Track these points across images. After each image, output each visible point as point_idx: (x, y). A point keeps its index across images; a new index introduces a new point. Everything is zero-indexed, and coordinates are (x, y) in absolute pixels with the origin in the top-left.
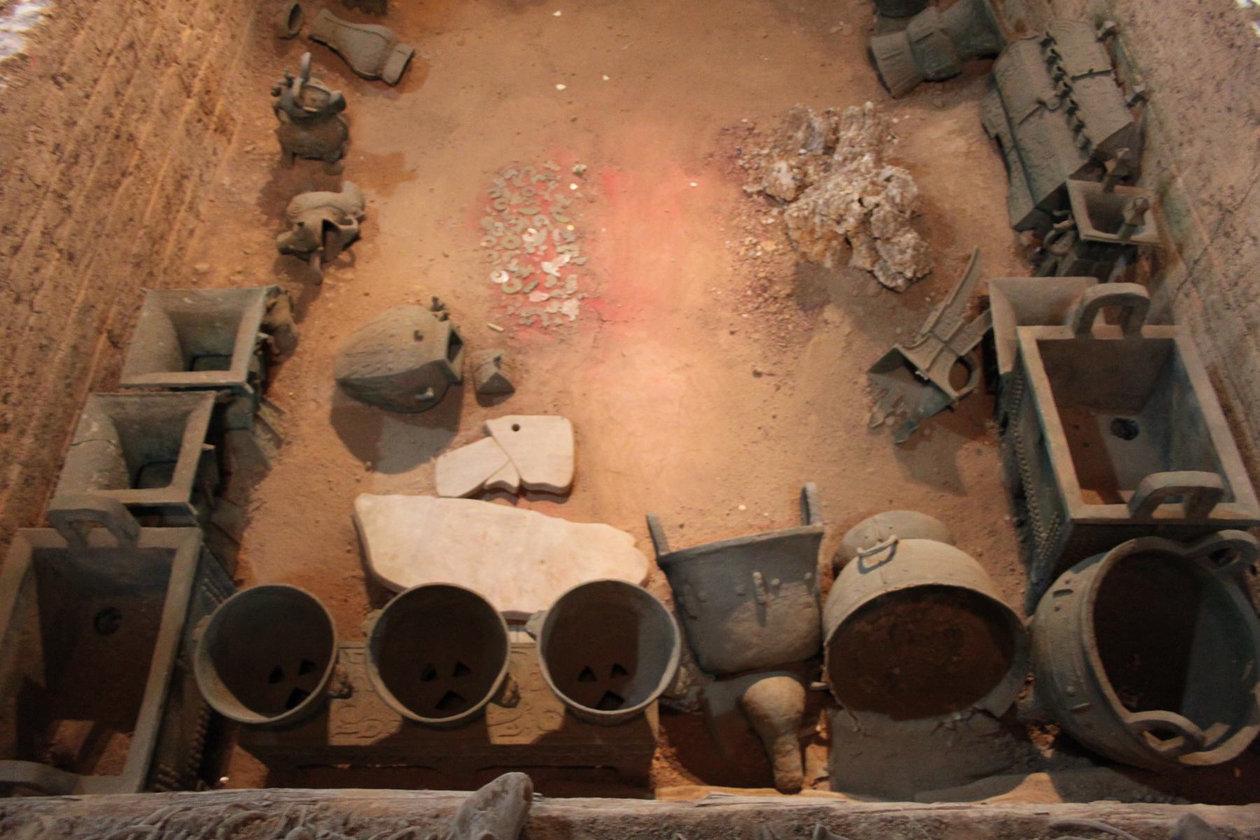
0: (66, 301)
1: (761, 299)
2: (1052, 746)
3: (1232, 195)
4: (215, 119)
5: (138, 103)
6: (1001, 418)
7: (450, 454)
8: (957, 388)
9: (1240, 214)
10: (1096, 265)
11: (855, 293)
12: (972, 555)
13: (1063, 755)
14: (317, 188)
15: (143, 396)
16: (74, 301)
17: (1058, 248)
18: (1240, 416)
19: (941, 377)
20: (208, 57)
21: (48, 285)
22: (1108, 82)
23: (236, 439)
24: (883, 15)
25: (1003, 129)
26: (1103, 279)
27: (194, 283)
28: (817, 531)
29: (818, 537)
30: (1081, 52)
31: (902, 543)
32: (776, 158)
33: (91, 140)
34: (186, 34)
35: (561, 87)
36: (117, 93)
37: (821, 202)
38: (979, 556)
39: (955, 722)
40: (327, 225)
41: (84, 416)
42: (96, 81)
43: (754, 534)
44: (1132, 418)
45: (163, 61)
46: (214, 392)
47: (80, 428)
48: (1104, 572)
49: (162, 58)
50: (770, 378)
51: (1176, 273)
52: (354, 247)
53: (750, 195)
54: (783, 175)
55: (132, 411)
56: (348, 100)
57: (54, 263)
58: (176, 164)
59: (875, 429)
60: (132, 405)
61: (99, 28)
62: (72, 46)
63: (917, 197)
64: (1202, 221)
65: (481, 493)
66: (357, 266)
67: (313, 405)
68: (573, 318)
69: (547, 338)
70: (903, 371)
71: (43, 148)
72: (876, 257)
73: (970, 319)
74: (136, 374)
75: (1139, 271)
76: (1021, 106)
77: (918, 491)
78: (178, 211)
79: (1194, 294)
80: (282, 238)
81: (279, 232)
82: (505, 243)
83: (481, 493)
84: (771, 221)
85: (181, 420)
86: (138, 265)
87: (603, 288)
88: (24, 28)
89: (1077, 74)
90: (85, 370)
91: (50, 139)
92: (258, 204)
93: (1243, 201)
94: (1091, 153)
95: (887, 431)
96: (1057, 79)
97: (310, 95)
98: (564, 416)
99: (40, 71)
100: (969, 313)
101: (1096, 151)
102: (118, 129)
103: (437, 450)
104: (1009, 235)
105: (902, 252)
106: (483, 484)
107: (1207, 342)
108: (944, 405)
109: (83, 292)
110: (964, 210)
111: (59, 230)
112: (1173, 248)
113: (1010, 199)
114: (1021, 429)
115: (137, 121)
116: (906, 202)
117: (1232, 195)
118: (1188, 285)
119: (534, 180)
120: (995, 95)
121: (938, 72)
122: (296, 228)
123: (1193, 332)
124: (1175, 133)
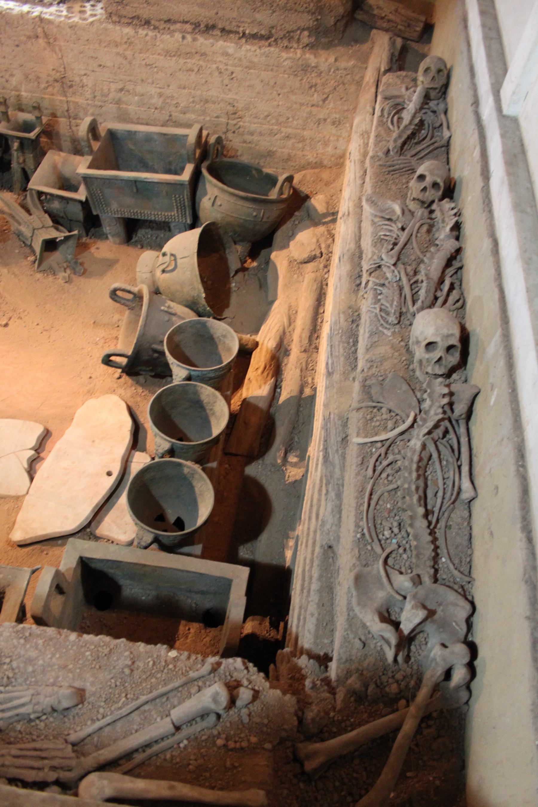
3: (57, 72)
9: (69, 74)
39: (235, 286)
65: (31, 473)
83: (31, 473)
93: (64, 68)
95: (73, 276)
106: (26, 470)
118: (73, 122)
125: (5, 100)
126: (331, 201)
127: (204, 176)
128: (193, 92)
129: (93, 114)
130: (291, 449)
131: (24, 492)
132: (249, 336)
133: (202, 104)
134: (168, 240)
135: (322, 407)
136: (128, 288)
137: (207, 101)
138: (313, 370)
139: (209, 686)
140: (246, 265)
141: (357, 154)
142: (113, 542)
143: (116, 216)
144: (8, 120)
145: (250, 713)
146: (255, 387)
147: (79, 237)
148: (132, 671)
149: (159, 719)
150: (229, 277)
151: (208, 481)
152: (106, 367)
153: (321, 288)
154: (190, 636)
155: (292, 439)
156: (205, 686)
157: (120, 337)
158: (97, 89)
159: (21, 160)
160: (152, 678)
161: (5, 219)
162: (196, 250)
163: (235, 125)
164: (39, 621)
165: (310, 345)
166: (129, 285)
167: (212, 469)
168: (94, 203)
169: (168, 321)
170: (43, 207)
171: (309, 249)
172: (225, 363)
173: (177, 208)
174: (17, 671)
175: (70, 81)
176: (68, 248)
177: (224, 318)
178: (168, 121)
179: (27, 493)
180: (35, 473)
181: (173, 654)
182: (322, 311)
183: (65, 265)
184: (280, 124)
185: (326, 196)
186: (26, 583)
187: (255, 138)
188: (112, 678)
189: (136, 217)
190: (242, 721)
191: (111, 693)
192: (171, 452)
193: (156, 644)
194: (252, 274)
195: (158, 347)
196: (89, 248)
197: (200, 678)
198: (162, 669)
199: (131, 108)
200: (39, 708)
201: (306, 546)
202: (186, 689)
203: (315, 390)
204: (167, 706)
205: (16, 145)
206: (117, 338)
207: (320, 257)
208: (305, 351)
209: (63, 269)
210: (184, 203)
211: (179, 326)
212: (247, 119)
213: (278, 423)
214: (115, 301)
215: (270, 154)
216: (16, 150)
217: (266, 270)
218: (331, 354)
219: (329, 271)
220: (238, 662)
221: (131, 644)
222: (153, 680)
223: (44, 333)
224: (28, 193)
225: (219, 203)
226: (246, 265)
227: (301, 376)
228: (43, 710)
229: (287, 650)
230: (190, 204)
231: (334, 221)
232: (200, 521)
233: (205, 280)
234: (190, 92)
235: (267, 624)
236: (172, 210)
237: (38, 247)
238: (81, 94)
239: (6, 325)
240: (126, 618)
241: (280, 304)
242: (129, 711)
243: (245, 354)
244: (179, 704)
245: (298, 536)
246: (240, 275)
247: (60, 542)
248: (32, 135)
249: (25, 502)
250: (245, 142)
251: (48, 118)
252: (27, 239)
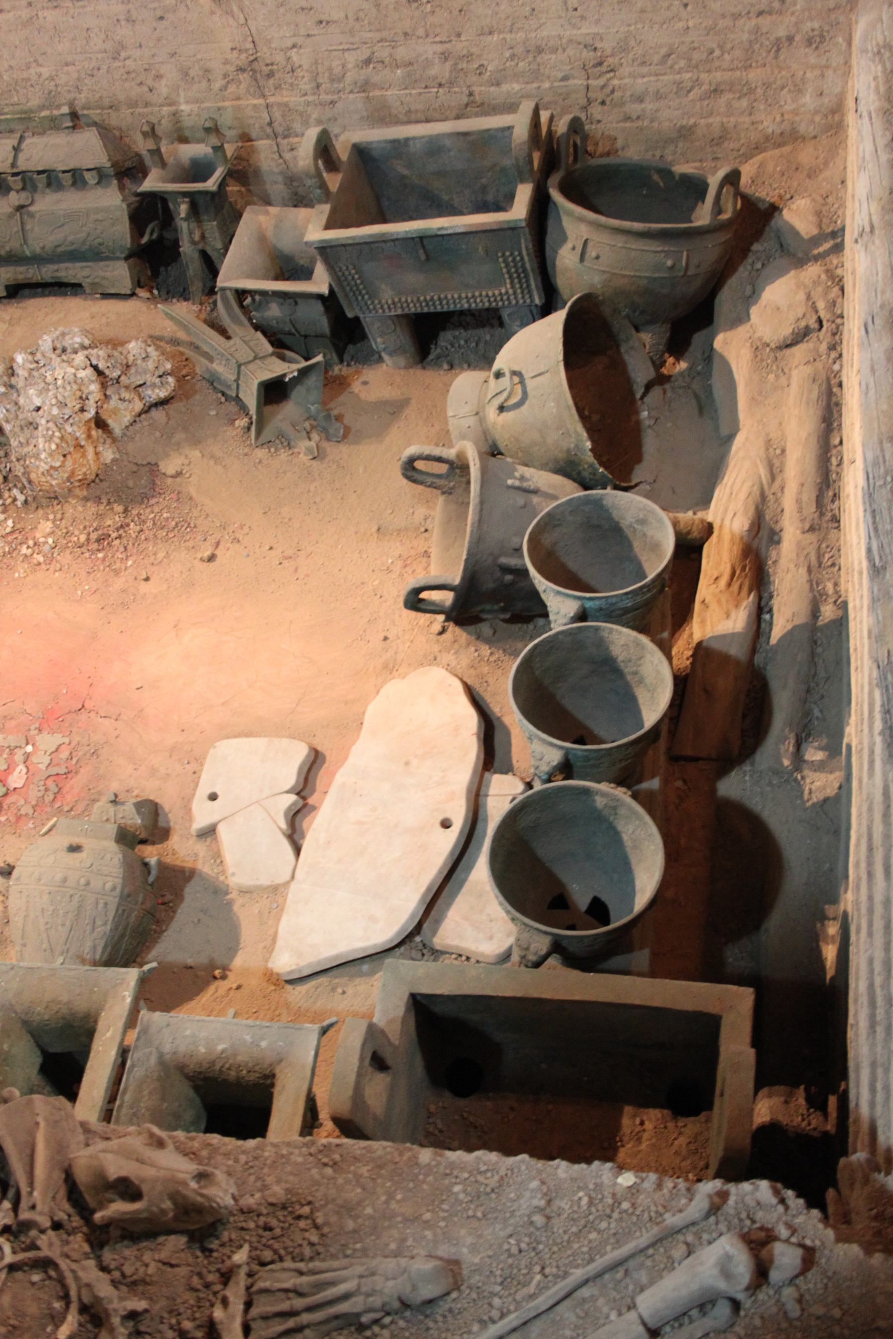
2: (678, 360)
9: (264, 53)
13: (687, 354)
39: (649, 417)
50: (221, 546)
65: (295, 838)
83: (295, 838)
89: (10, 160)
95: (325, 444)
106: (284, 833)
125: (153, 129)
126: (824, 209)
127: (555, 204)
128: (508, 36)
129: (319, 122)
130: (808, 735)
131: (287, 877)
132: (690, 513)
133: (530, 58)
134: (501, 347)
135: (866, 641)
136: (437, 451)
137: (539, 50)
138: (833, 565)
139: (710, 1243)
140: (664, 371)
141: (873, 97)
142: (468, 958)
143: (393, 313)
144: (163, 164)
145: (802, 1296)
146: (719, 616)
147: (327, 366)
148: (549, 1218)
149: (613, 1316)
150: (633, 401)
151: (648, 819)
152: (413, 614)
153: (830, 393)
154: (646, 1136)
155: (808, 713)
156: (701, 1244)
157: (434, 552)
158: (320, 70)
159: (197, 237)
160: (590, 1232)
161: (182, 354)
162: (561, 357)
163: (603, 87)
164: (348, 1127)
165: (822, 514)
166: (437, 445)
167: (651, 794)
168: (346, 295)
169: (524, 506)
170: (250, 319)
171: (792, 317)
172: (651, 576)
173: (511, 277)
174: (326, 1230)
175: (267, 65)
176: (308, 390)
177: (636, 485)
178: (467, 105)
179: (293, 877)
180: (303, 837)
181: (627, 1179)
182: (837, 442)
183: (307, 425)
184: (697, 67)
185: (814, 200)
186: (313, 1053)
187: (649, 106)
188: (511, 1236)
189: (432, 309)
190: (785, 1313)
191: (511, 1266)
192: (566, 768)
193: (589, 1161)
194: (680, 387)
195: (512, 562)
196: (349, 385)
197: (687, 1227)
198: (608, 1211)
199: (392, 94)
200: (376, 1301)
201: (870, 934)
202: (662, 1250)
203: (844, 606)
204: (626, 1287)
205: (183, 209)
206: (427, 554)
207: (819, 329)
208: (812, 529)
209: (304, 433)
210: (523, 266)
211: (549, 514)
212: (626, 70)
213: (775, 685)
214: (414, 481)
215: (685, 133)
216: (185, 219)
217: (707, 374)
218: (876, 530)
219: (841, 355)
220: (762, 1190)
221: (540, 1164)
222: (593, 1236)
223: (285, 562)
224: (218, 297)
225: (594, 254)
226: (664, 371)
227: (810, 581)
228: (383, 1306)
229: (859, 1156)
230: (536, 265)
231: (839, 248)
232: (641, 900)
233: (586, 413)
234: (505, 39)
235: (802, 1101)
236: (497, 282)
237: (251, 398)
238: (291, 85)
239: (212, 558)
240: (512, 1109)
241: (747, 439)
242: (551, 1302)
243: (689, 550)
244: (652, 1282)
245: (845, 915)
246: (656, 391)
247: (365, 967)
248: (211, 184)
249: (290, 896)
250: (628, 118)
251: (235, 145)
252: (229, 387)
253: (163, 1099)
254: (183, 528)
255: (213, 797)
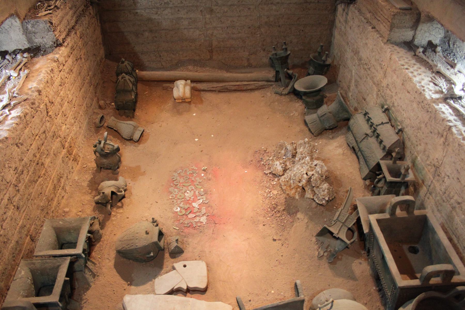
0: (15, 224)
1: (274, 212)
4: (73, 156)
5: (46, 152)
6: (367, 250)
7: (160, 277)
8: (349, 240)
9: (442, 168)
10: (394, 190)
11: (308, 207)
12: (363, 304)
14: (109, 179)
15: (43, 260)
16: (18, 224)
17: (380, 185)
18: (456, 241)
19: (343, 236)
20: (71, 135)
21: (9, 219)
22: (389, 126)
23: (78, 275)
24: (308, 108)
25: (355, 144)
26: (398, 195)
27: (63, 216)
28: (302, 299)
29: (303, 301)
30: (378, 116)
31: (335, 301)
32: (275, 160)
33: (28, 165)
34: (64, 127)
35: (196, 140)
36: (38, 149)
37: (292, 175)
38: (365, 304)
40: (113, 193)
41: (19, 269)
42: (31, 145)
43: (278, 302)
44: (416, 246)
45: (55, 137)
46: (70, 257)
47: (17, 273)
48: (415, 307)
49: (55, 136)
51: (423, 191)
52: (123, 201)
53: (267, 174)
54: (278, 166)
55: (38, 266)
56: (120, 148)
57: (12, 210)
58: (58, 173)
59: (320, 258)
60: (38, 263)
61: (34, 127)
62: (23, 133)
63: (327, 171)
64: (429, 171)
65: (172, 292)
66: (124, 207)
67: (107, 261)
68: (204, 223)
69: (196, 231)
70: (329, 235)
71: (10, 169)
72: (315, 194)
73: (351, 214)
74: (40, 251)
75: (410, 191)
76: (360, 136)
77: (339, 280)
78: (58, 190)
79: (431, 197)
80: (96, 198)
81: (95, 196)
82: (178, 196)
83: (172, 292)
84: (275, 183)
85: (56, 269)
86: (43, 210)
87: (215, 212)
88: (8, 128)
89: (378, 124)
90: (20, 251)
91: (14, 166)
92: (87, 186)
94: (387, 150)
95: (325, 258)
96: (371, 126)
97: (107, 146)
98: (203, 260)
99: (12, 142)
100: (350, 211)
101: (388, 150)
102: (38, 161)
103: (155, 276)
104: (361, 182)
105: (324, 191)
107: (439, 215)
108: (345, 246)
109: (22, 221)
110: (344, 174)
111: (14, 198)
112: (421, 182)
113: (360, 169)
114: (375, 253)
115: (45, 158)
116: (323, 173)
117: (438, 162)
118: (428, 195)
119: (188, 173)
120: (350, 133)
121: (329, 127)
122: (101, 194)
123: (433, 211)
124: (414, 142)
253: (50, 269)
254: (284, 228)
255: (185, 266)
